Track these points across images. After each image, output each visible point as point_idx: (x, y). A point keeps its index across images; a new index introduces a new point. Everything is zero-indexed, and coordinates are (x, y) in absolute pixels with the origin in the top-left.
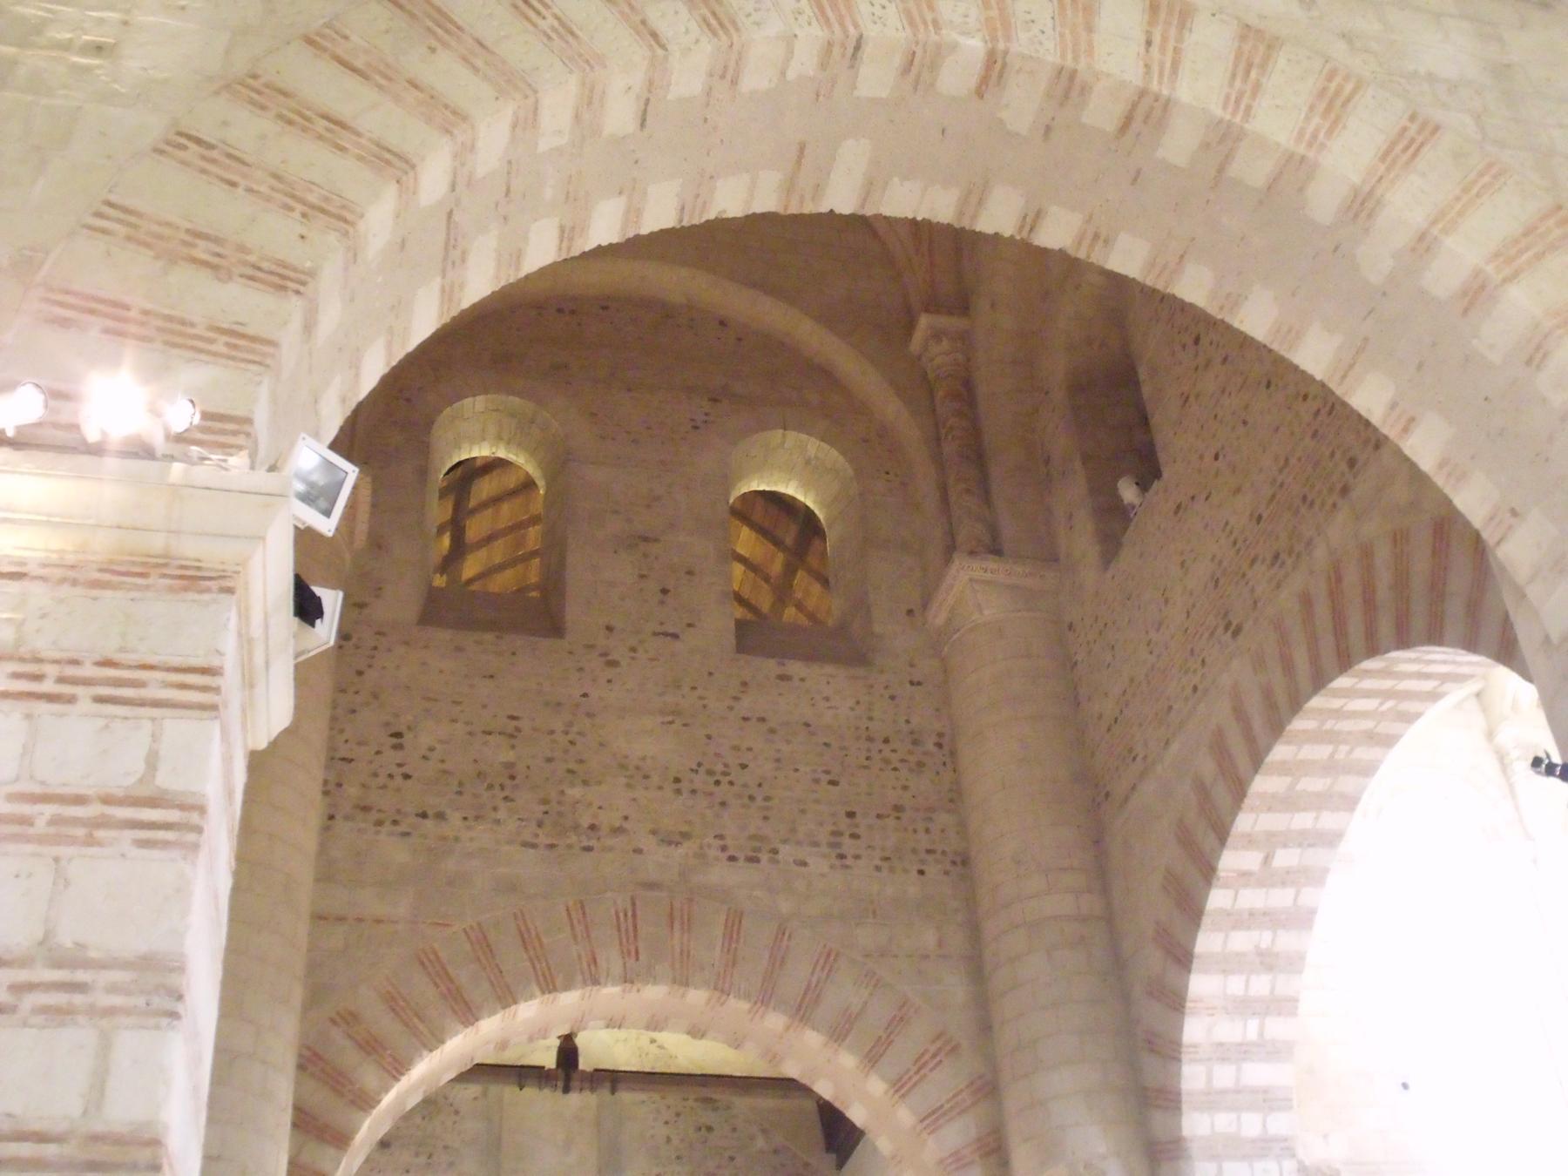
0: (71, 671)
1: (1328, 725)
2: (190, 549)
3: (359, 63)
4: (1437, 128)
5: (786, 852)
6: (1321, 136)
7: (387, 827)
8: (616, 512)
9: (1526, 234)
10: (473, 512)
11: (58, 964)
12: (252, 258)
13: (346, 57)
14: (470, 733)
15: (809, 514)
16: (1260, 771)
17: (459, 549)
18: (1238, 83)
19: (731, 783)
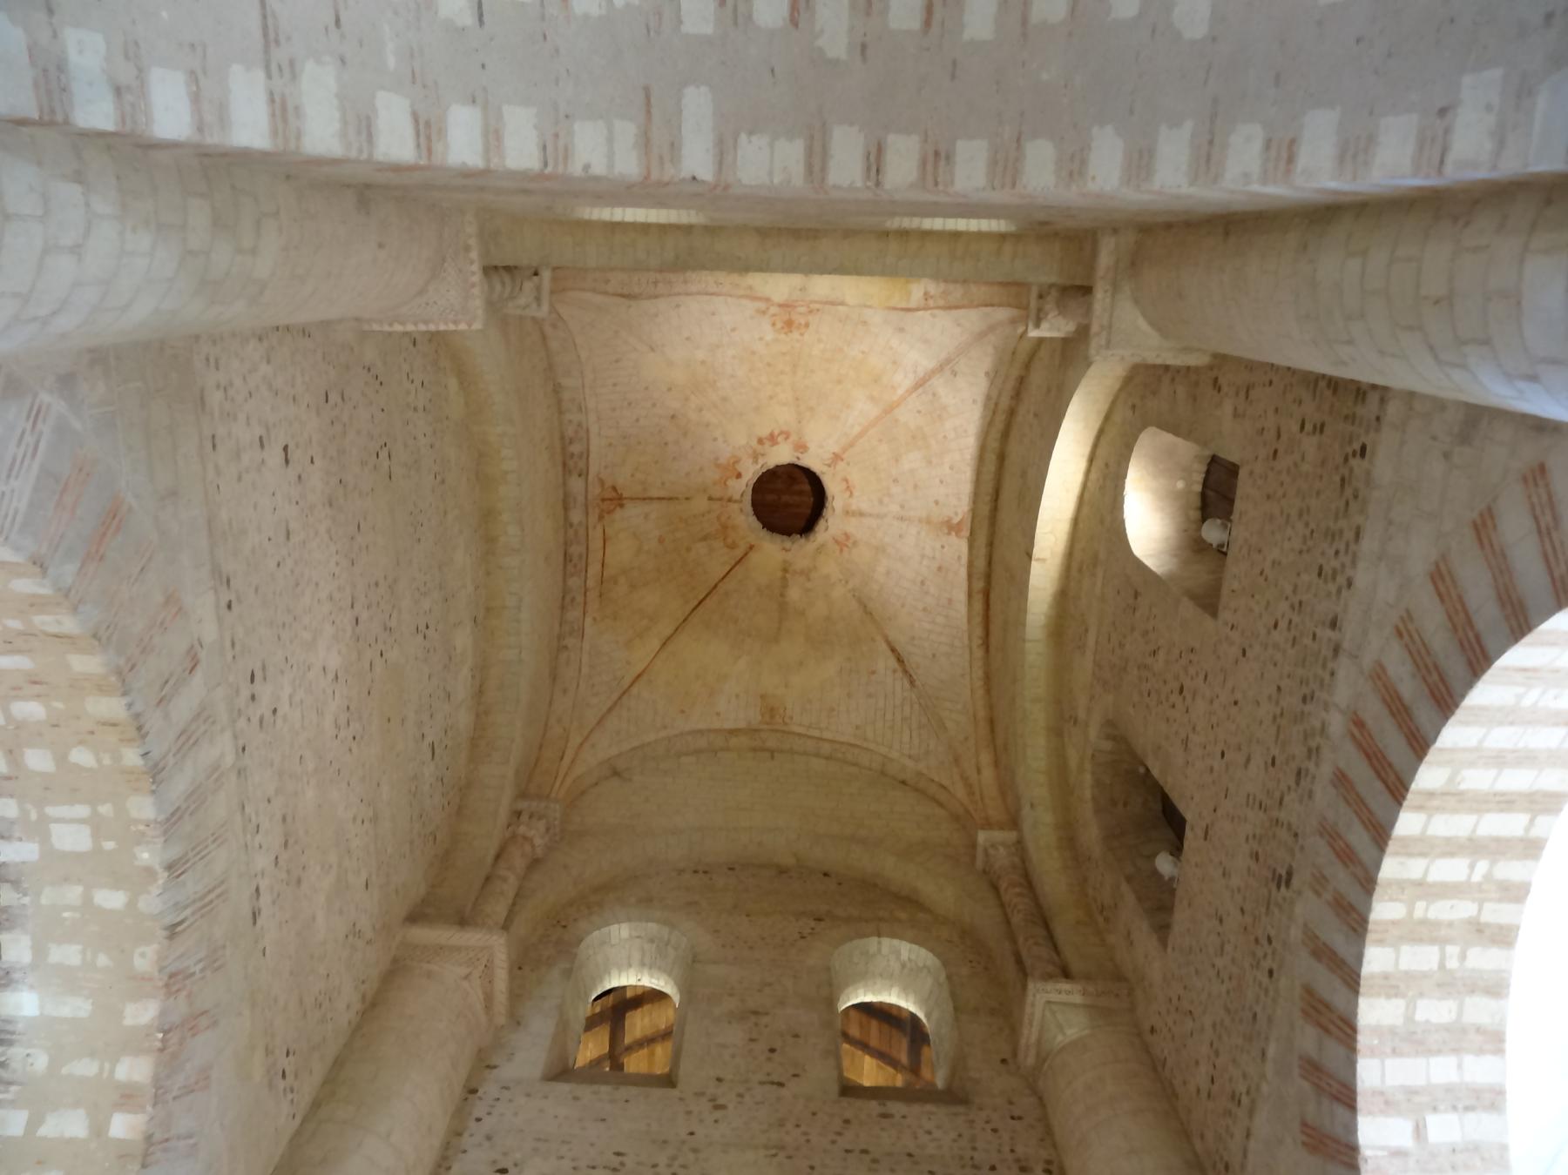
1: (1420, 909)
8: (731, 995)
10: (629, 1049)
14: (575, 1168)
15: (913, 1017)
16: (1362, 990)
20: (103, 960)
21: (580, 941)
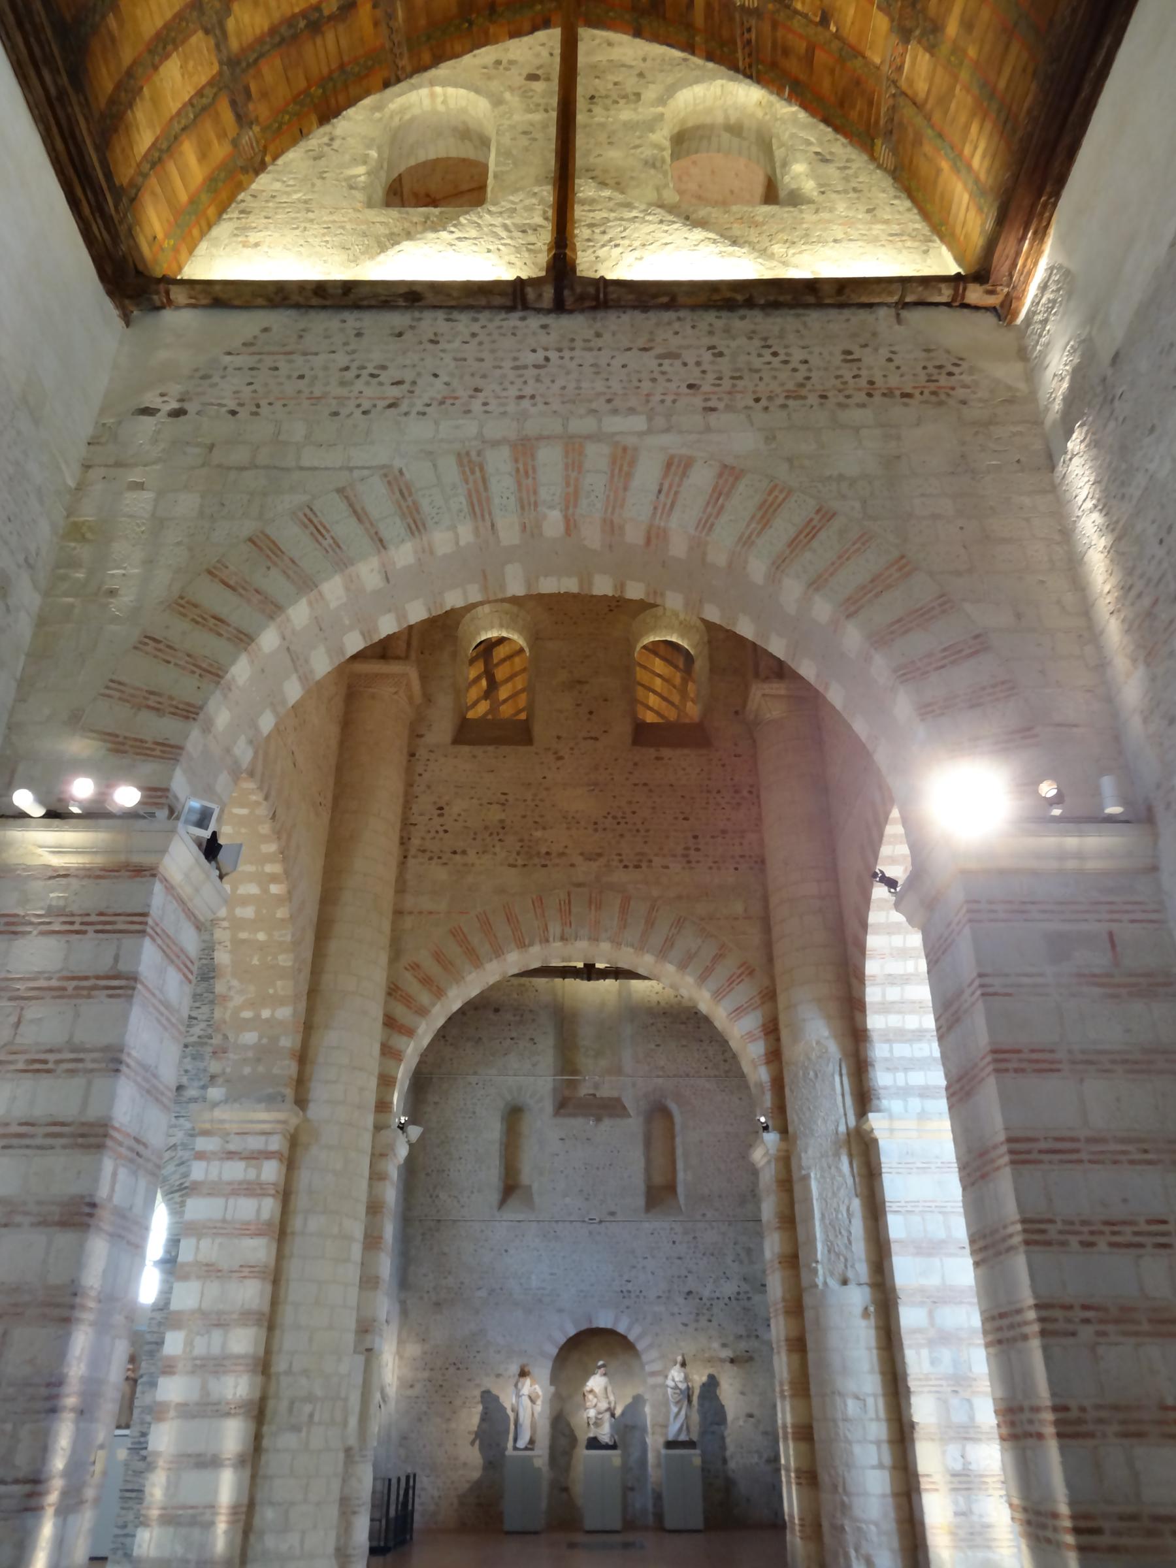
0: (86, 919)
2: (137, 859)
3: (232, 583)
4: (834, 514)
5: (657, 861)
6: (754, 536)
7: (435, 860)
8: (563, 668)
9: (872, 581)
10: (498, 665)
11: (73, 1051)
12: (174, 703)
13: (226, 580)
14: (481, 805)
17: (493, 685)
18: (709, 509)
19: (626, 823)
20: (243, 830)
21: (458, 624)
